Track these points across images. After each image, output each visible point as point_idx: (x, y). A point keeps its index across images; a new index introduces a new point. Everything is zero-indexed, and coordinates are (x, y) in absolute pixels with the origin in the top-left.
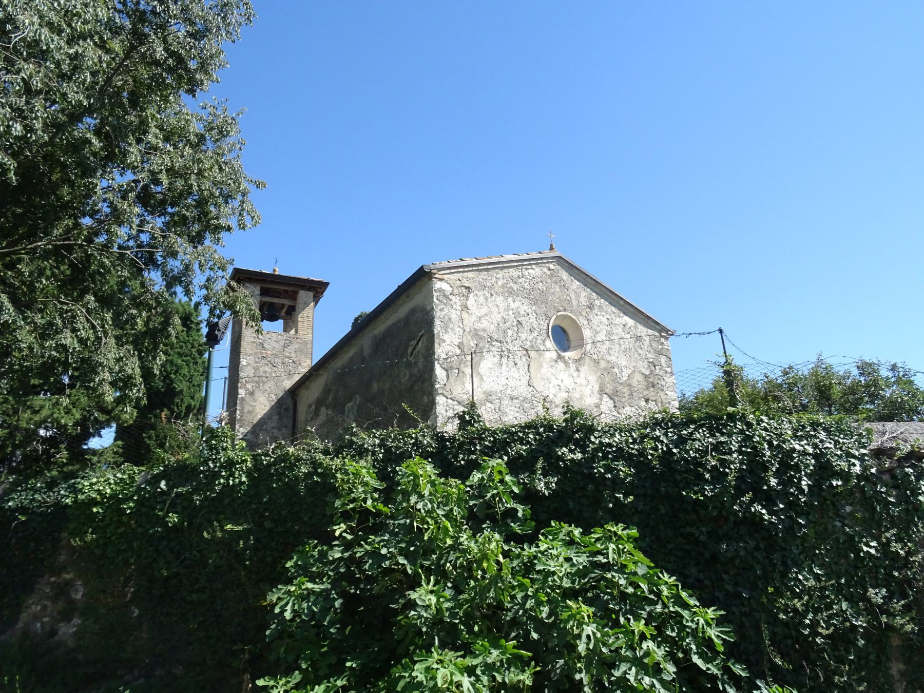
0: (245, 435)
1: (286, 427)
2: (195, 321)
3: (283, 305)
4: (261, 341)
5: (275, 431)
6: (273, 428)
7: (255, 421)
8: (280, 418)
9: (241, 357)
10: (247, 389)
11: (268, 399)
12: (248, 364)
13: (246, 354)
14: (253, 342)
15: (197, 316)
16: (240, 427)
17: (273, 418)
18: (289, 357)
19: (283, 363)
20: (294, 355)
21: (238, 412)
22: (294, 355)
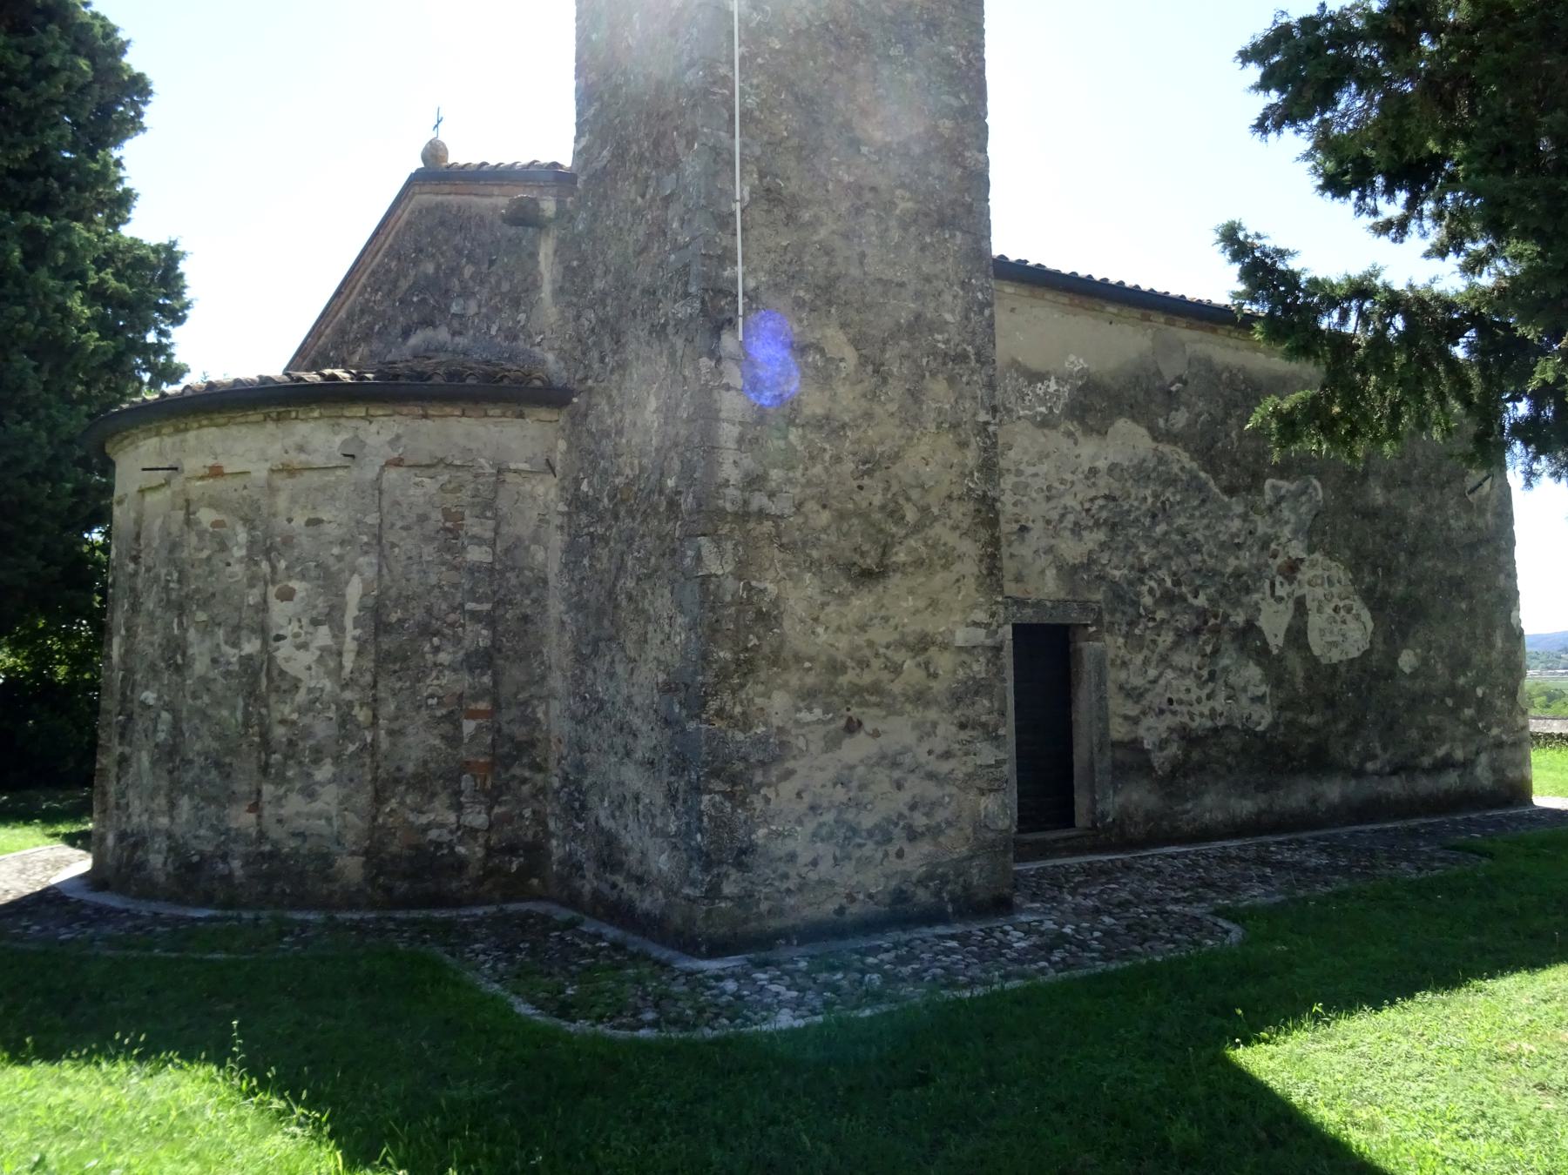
1: (1230, 332)
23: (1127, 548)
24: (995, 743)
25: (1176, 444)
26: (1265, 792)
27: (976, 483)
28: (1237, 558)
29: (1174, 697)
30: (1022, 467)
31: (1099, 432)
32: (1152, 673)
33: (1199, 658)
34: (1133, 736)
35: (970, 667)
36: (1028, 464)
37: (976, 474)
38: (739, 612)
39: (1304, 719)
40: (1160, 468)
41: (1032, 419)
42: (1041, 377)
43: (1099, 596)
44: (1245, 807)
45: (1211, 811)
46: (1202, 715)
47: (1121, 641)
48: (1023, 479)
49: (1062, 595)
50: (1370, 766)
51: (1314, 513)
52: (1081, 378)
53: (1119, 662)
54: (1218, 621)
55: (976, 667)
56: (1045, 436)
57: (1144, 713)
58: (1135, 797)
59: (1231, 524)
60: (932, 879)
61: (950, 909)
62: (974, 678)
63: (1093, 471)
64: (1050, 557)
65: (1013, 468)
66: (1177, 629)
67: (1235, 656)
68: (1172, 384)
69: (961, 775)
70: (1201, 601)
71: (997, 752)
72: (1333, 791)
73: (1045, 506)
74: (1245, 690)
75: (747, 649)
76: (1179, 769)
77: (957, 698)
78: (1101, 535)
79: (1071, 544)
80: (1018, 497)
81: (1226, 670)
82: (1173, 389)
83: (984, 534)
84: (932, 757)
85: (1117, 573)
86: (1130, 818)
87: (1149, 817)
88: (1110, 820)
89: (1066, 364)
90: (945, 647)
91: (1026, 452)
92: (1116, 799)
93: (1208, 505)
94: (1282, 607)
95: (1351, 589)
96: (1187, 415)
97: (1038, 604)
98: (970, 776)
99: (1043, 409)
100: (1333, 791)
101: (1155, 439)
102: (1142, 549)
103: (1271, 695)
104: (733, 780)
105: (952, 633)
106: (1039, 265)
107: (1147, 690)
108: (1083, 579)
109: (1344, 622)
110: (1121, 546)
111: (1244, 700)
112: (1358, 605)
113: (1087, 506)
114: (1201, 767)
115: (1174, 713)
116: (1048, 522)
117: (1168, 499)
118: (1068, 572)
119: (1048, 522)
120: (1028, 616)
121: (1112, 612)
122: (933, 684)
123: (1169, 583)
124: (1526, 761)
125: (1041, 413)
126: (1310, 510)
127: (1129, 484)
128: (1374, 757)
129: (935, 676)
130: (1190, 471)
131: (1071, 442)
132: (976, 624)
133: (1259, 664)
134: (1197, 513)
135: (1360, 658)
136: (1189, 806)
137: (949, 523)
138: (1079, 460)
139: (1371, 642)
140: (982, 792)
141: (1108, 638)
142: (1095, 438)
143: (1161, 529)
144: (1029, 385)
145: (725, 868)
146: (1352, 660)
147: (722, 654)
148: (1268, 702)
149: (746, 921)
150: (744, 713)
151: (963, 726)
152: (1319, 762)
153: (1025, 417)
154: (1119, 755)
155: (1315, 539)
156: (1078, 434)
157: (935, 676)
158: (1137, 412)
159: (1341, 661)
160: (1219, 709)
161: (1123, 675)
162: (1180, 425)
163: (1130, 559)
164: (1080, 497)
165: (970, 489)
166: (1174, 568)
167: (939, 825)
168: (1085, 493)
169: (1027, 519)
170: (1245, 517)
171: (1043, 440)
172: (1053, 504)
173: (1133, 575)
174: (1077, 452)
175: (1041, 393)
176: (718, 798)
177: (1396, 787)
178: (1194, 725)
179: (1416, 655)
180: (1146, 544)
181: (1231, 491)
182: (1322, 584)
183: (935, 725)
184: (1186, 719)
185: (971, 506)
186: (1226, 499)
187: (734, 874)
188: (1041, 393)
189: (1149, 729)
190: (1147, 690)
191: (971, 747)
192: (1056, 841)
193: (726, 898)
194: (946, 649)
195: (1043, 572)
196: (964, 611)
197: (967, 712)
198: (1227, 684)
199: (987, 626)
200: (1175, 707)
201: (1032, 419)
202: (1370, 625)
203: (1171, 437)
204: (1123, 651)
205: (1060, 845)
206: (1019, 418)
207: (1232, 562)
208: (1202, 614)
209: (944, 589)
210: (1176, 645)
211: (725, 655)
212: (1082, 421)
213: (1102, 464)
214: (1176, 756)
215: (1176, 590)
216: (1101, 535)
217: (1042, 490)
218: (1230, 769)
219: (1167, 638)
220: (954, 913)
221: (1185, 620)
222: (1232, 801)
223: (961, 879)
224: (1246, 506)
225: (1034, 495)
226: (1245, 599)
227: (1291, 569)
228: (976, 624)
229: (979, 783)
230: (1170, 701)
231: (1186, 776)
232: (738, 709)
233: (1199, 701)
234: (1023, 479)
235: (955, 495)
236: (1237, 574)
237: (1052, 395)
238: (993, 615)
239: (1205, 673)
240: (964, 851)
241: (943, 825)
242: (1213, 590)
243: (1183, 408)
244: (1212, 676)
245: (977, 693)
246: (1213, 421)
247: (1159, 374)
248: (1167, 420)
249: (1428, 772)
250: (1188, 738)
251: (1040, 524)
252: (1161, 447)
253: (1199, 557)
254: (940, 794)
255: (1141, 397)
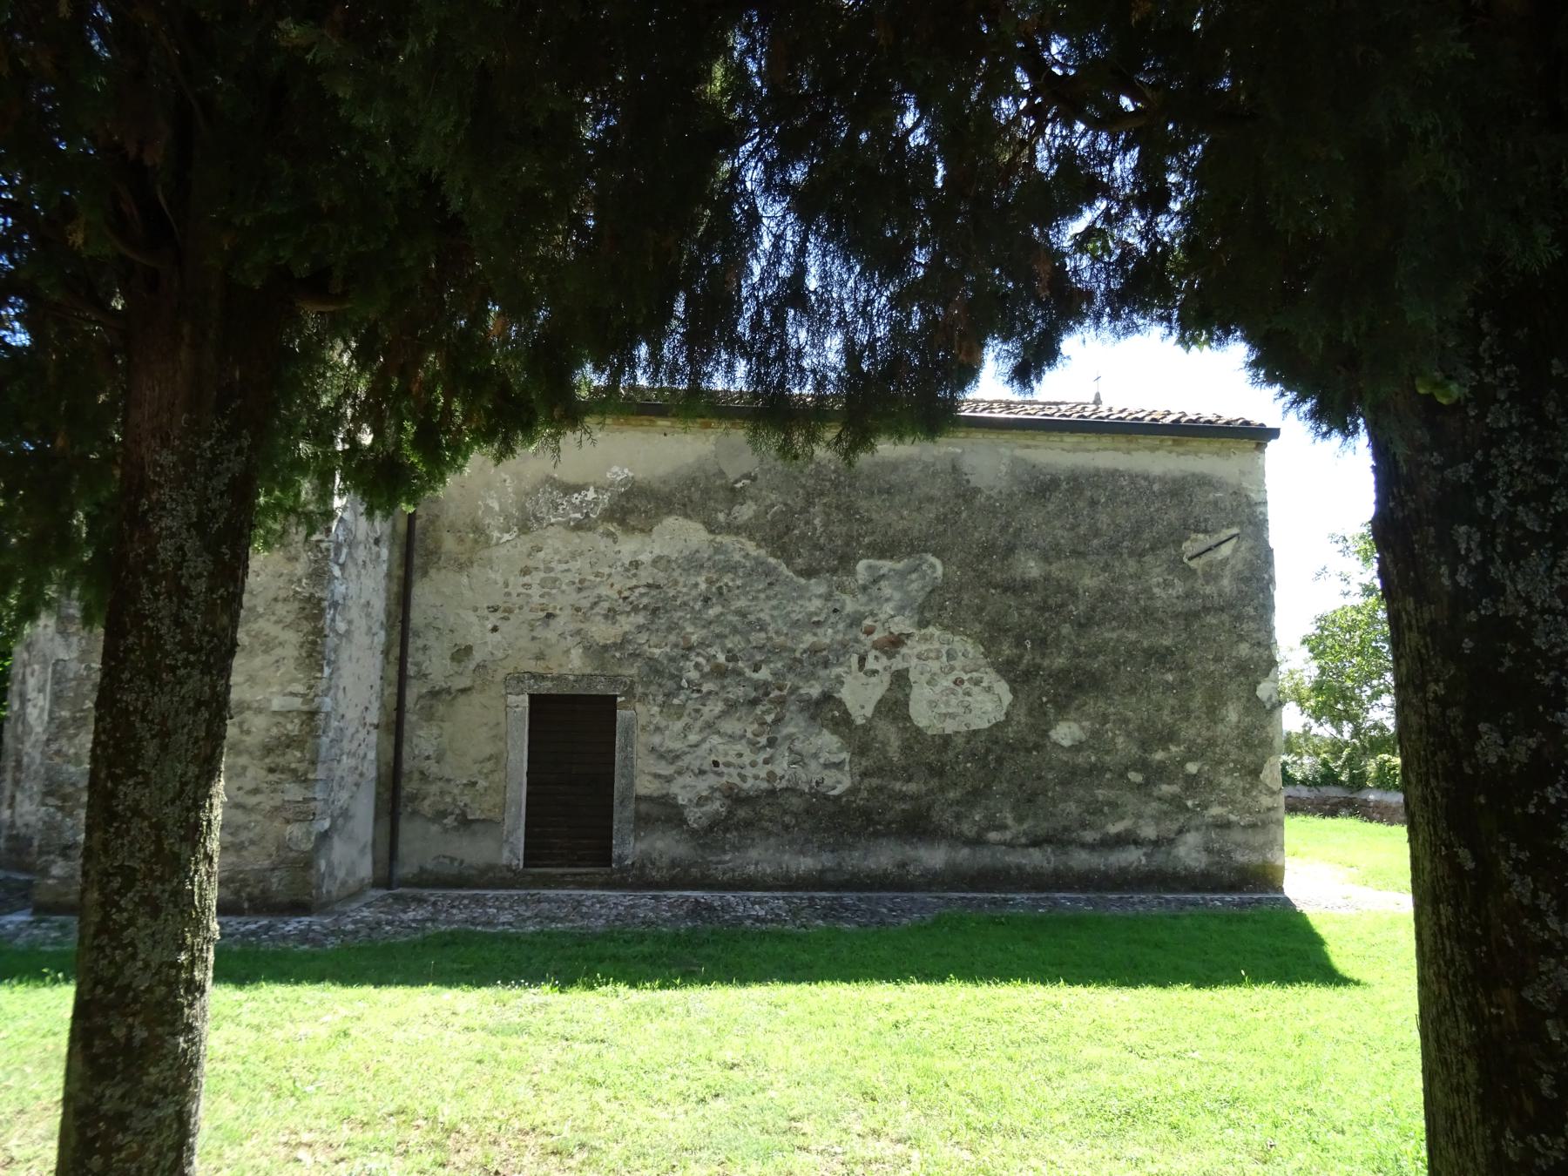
23: (670, 629)
24: (304, 785)
25: (737, 534)
26: (832, 851)
27: (305, 588)
28: (815, 634)
29: (721, 760)
31: (642, 531)
32: (693, 738)
33: (756, 726)
34: (664, 792)
35: (285, 727)
36: (560, 561)
37: (304, 581)
38: (79, 685)
39: (898, 786)
40: (717, 558)
42: (578, 488)
43: (634, 671)
44: (805, 864)
45: (756, 864)
46: (756, 777)
47: (656, 709)
48: (552, 575)
49: (588, 671)
50: (993, 836)
51: (928, 589)
52: (625, 485)
53: (652, 727)
54: (785, 692)
55: (290, 727)
57: (680, 773)
58: (660, 845)
59: (807, 604)
60: (233, 882)
61: (246, 905)
62: (287, 735)
63: (636, 564)
64: (578, 639)
66: (726, 701)
67: (803, 724)
68: (736, 482)
69: (268, 808)
70: (764, 674)
71: (304, 791)
72: (935, 857)
73: (575, 596)
74: (815, 756)
75: (82, 711)
76: (716, 825)
77: (268, 750)
78: (640, 619)
79: (603, 627)
81: (791, 738)
82: (739, 485)
83: (307, 626)
84: (241, 792)
85: (657, 651)
86: (653, 863)
87: (673, 864)
88: (629, 862)
89: (608, 475)
90: (259, 711)
92: (638, 845)
93: (777, 588)
94: (874, 680)
95: (982, 661)
96: (755, 507)
97: (560, 678)
98: (276, 809)
99: (578, 515)
100: (935, 857)
101: (711, 532)
102: (690, 629)
103: (850, 762)
104: (64, 798)
105: (269, 701)
107: (685, 753)
108: (614, 656)
109: (968, 694)
110: (663, 627)
111: (813, 765)
112: (989, 677)
113: (626, 594)
114: (748, 824)
115: (720, 775)
117: (726, 585)
118: (597, 652)
120: (546, 687)
121: (648, 684)
122: (248, 739)
123: (721, 658)
124: (1276, 843)
125: (575, 519)
126: (923, 588)
127: (676, 574)
128: (1002, 827)
129: (248, 732)
130: (756, 559)
131: (610, 541)
132: (295, 695)
133: (834, 732)
134: (762, 596)
135: (990, 729)
136: (727, 858)
137: (274, 618)
138: (619, 556)
139: (1007, 714)
140: (288, 822)
141: (638, 706)
142: (638, 537)
143: (712, 612)
144: (565, 495)
145: (52, 857)
146: (975, 732)
147: (63, 713)
148: (847, 768)
149: (66, 894)
150: (76, 754)
151: (271, 770)
152: (917, 827)
153: (559, 523)
154: (644, 807)
155: (927, 615)
156: (618, 533)
157: (248, 732)
158: (687, 508)
159: (957, 733)
160: (779, 772)
161: (656, 739)
162: (746, 517)
163: (672, 638)
164: (617, 587)
165: (296, 592)
166: (730, 646)
167: (242, 842)
168: (620, 582)
169: (555, 608)
170: (828, 597)
171: (578, 541)
173: (676, 652)
174: (617, 549)
175: (577, 502)
176: (52, 810)
177: (1037, 859)
178: (746, 786)
179: (1083, 728)
180: (694, 624)
181: (809, 573)
182: (938, 658)
183: (245, 768)
184: (737, 780)
185: (296, 605)
186: (803, 581)
187: (60, 862)
188: (577, 502)
189: (684, 787)
190: (685, 753)
191: (280, 787)
192: (563, 875)
193: (54, 877)
194: (260, 712)
195: (567, 651)
196: (282, 684)
197: (277, 760)
198: (791, 750)
199: (303, 696)
200: (722, 768)
201: (566, 525)
202: (1008, 698)
203: (733, 529)
204: (658, 718)
205: (569, 879)
206: (552, 525)
207: (808, 639)
208: (764, 687)
209: (263, 668)
210: (724, 714)
211: (65, 714)
212: (622, 522)
213: (645, 557)
214: (717, 812)
215: (731, 665)
216: (640, 619)
217: (574, 583)
218: (786, 827)
219: (714, 708)
220: (249, 908)
221: (738, 692)
222: (786, 857)
223: (261, 885)
224: (830, 586)
225: (564, 587)
226: (822, 673)
227: (894, 644)
228: (295, 695)
229: (285, 814)
230: (716, 764)
231: (727, 830)
232: (72, 751)
233: (753, 764)
234: (552, 575)
235: (280, 598)
236: (813, 651)
237: (589, 503)
238: (310, 687)
239: (763, 740)
240: (267, 863)
241: (247, 844)
242: (779, 665)
243: (750, 502)
244: (771, 742)
245: (288, 746)
246: (789, 511)
247: (721, 474)
248: (729, 515)
249: (1092, 847)
250: (735, 797)
252: (719, 538)
253: (763, 635)
254: (247, 820)
255: (696, 496)
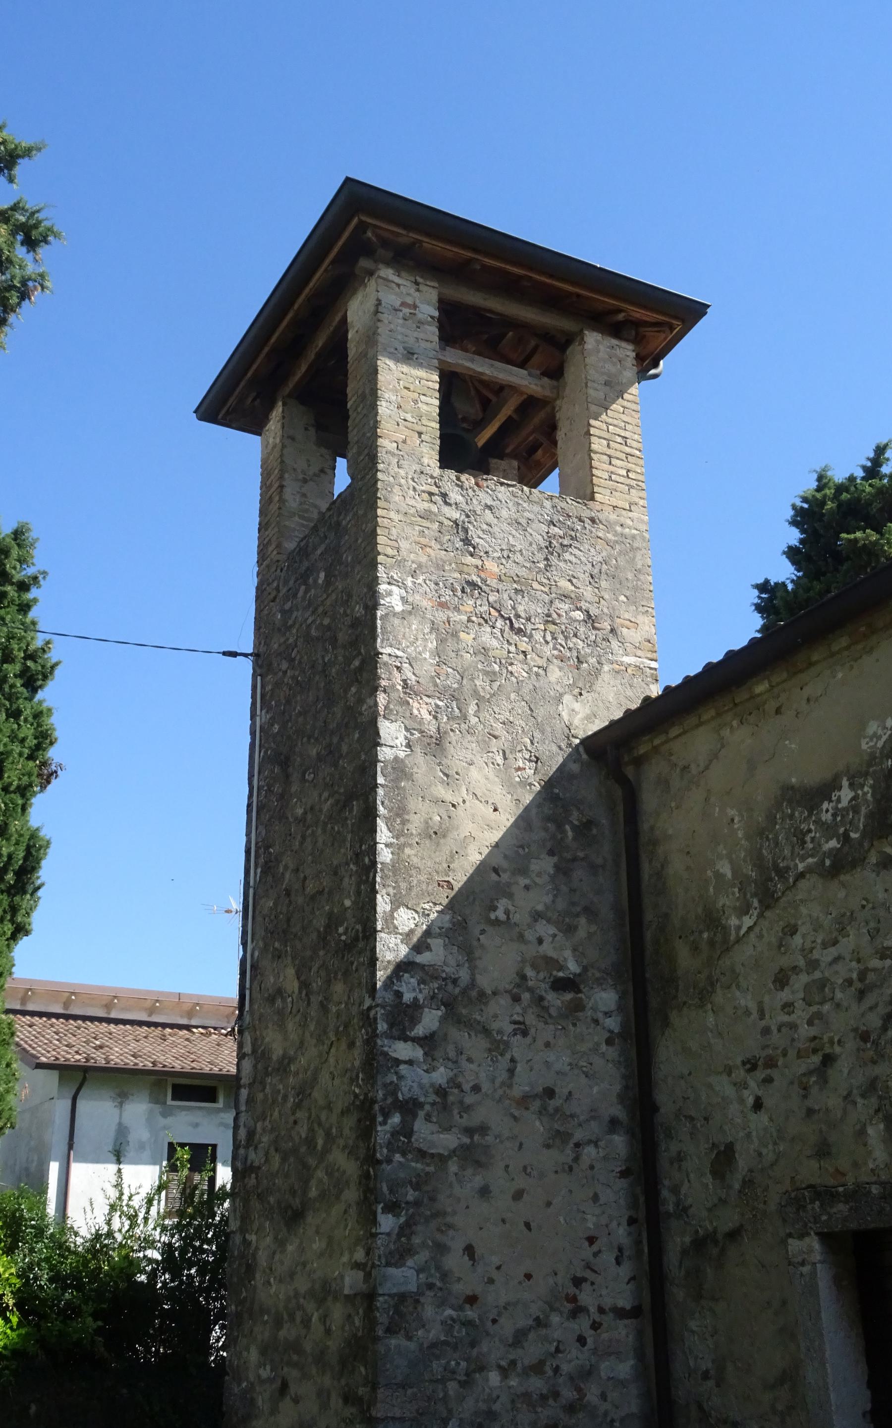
0: (420, 947)
1: (590, 912)
2: (17, 577)
3: (500, 389)
4: (456, 515)
5: (545, 929)
6: (537, 916)
7: (459, 879)
8: (563, 870)
9: (381, 572)
10: (413, 726)
11: (505, 769)
12: (413, 610)
13: (400, 564)
14: (426, 516)
15: (22, 560)
16: (397, 903)
17: (535, 866)
18: (574, 600)
19: (548, 620)
20: (588, 593)
21: (383, 834)
22: (588, 593)
30: (816, 955)
36: (825, 945)
41: (819, 870)
42: (827, 790)
56: (843, 885)
64: (874, 1101)
65: (802, 963)
80: (815, 1008)
91: (817, 927)
97: (856, 1194)
106: (751, 640)
116: (864, 1037)
119: (864, 1037)
153: (810, 870)
169: (831, 1042)
171: (842, 894)
172: (870, 1000)
201: (819, 870)
251: (851, 1044)
